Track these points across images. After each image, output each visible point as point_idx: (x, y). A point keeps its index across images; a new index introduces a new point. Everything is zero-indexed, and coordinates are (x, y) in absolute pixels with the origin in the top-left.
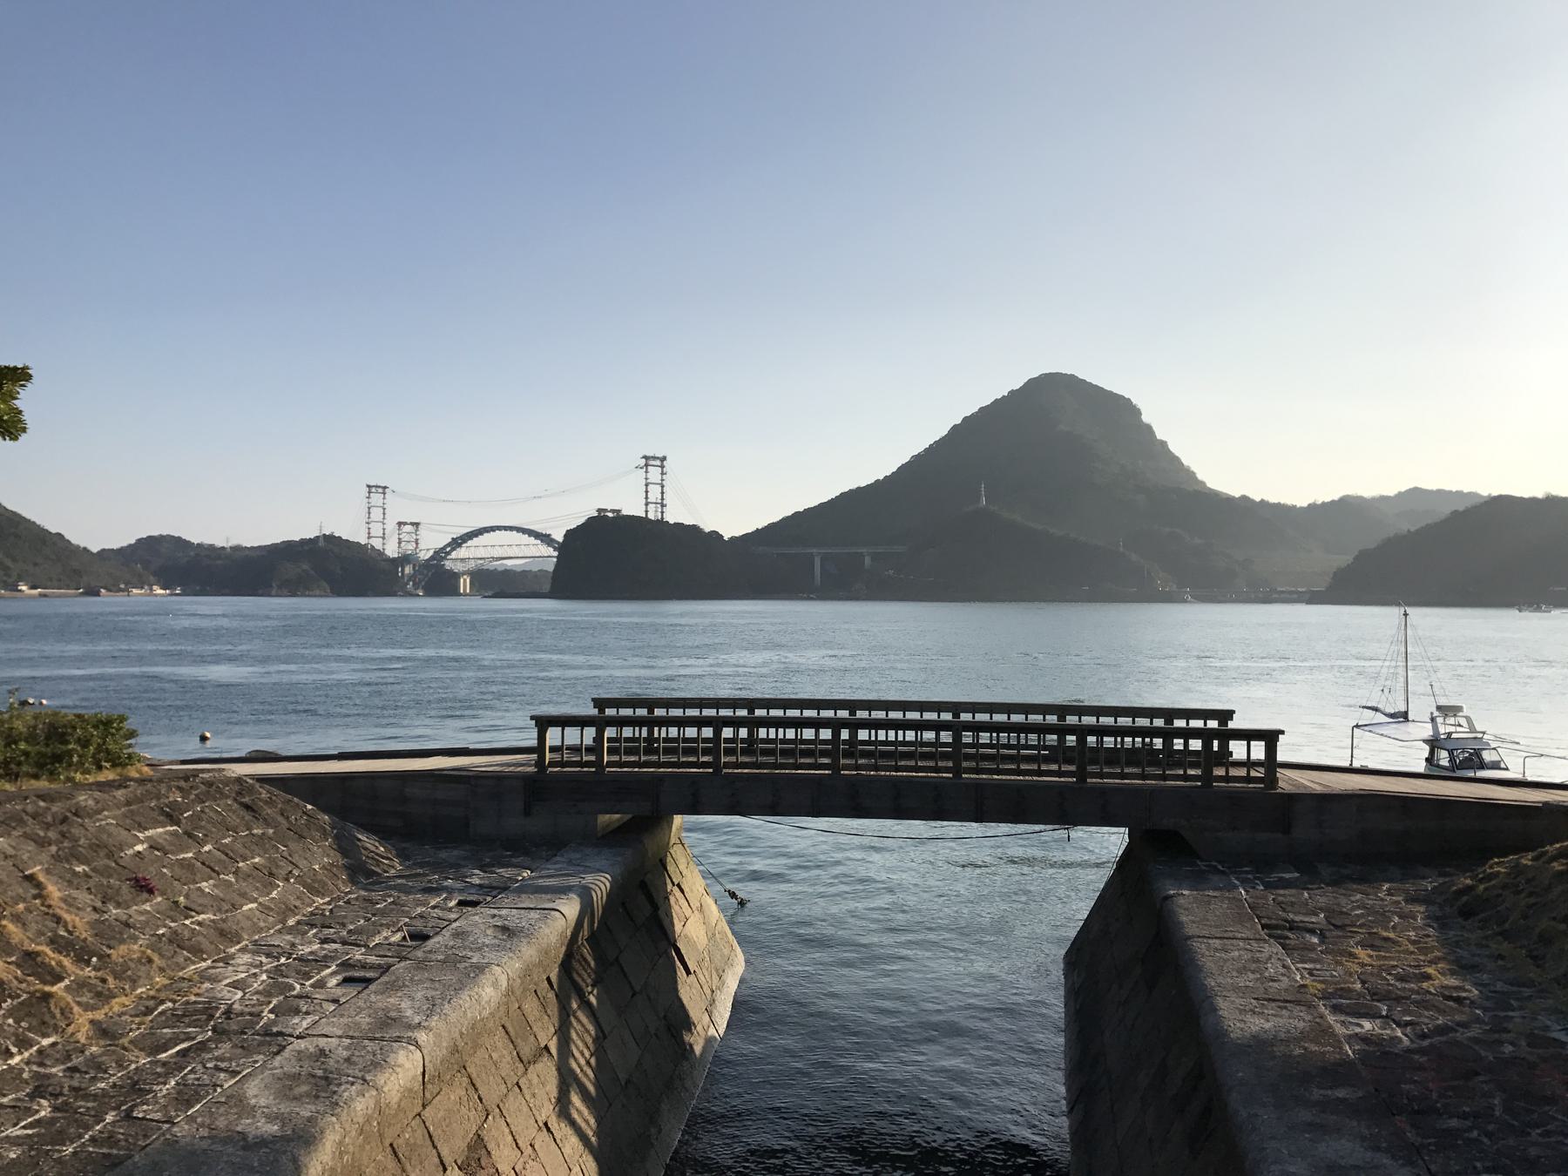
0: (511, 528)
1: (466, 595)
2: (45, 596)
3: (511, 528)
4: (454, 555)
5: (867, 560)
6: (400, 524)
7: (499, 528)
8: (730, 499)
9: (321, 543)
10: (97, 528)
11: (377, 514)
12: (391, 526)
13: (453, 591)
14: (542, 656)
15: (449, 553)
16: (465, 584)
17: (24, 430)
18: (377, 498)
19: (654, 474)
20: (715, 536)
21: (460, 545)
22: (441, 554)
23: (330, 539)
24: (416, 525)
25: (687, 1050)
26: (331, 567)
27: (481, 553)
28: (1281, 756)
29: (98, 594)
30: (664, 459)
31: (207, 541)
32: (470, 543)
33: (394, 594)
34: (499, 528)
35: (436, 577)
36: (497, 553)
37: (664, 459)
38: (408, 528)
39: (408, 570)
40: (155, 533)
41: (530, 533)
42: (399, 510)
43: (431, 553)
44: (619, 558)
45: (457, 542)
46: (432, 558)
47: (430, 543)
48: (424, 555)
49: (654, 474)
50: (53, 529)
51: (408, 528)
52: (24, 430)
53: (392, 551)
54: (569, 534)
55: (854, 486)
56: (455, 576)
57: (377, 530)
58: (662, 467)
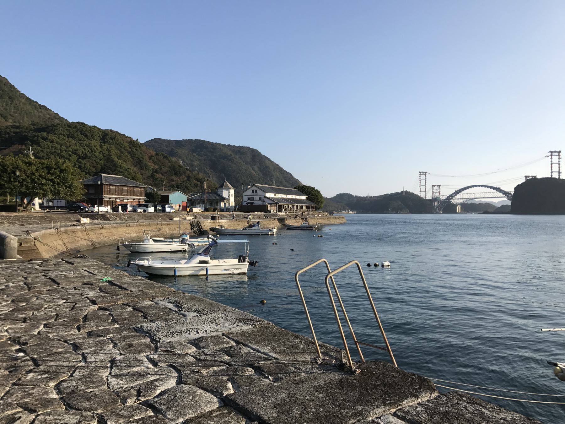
0: (482, 186)
1: (459, 213)
3: (482, 186)
4: (456, 197)
6: (433, 186)
7: (476, 186)
9: (404, 194)
11: (423, 183)
12: (429, 187)
13: (454, 212)
15: (454, 197)
16: (459, 208)
18: (423, 177)
19: (555, 159)
21: (458, 193)
22: (450, 197)
23: (406, 192)
24: (439, 186)
25: (369, 403)
27: (469, 196)
28: (209, 273)
30: (560, 152)
31: (359, 195)
32: (463, 192)
33: (433, 213)
34: (476, 186)
35: (447, 206)
36: (472, 196)
37: (560, 152)
38: (436, 187)
40: (342, 193)
41: (491, 187)
42: (431, 181)
45: (457, 192)
46: (447, 199)
47: (444, 194)
48: (443, 198)
49: (555, 159)
51: (436, 187)
53: (429, 196)
54: (518, 188)
56: (455, 206)
57: (423, 189)
58: (559, 155)
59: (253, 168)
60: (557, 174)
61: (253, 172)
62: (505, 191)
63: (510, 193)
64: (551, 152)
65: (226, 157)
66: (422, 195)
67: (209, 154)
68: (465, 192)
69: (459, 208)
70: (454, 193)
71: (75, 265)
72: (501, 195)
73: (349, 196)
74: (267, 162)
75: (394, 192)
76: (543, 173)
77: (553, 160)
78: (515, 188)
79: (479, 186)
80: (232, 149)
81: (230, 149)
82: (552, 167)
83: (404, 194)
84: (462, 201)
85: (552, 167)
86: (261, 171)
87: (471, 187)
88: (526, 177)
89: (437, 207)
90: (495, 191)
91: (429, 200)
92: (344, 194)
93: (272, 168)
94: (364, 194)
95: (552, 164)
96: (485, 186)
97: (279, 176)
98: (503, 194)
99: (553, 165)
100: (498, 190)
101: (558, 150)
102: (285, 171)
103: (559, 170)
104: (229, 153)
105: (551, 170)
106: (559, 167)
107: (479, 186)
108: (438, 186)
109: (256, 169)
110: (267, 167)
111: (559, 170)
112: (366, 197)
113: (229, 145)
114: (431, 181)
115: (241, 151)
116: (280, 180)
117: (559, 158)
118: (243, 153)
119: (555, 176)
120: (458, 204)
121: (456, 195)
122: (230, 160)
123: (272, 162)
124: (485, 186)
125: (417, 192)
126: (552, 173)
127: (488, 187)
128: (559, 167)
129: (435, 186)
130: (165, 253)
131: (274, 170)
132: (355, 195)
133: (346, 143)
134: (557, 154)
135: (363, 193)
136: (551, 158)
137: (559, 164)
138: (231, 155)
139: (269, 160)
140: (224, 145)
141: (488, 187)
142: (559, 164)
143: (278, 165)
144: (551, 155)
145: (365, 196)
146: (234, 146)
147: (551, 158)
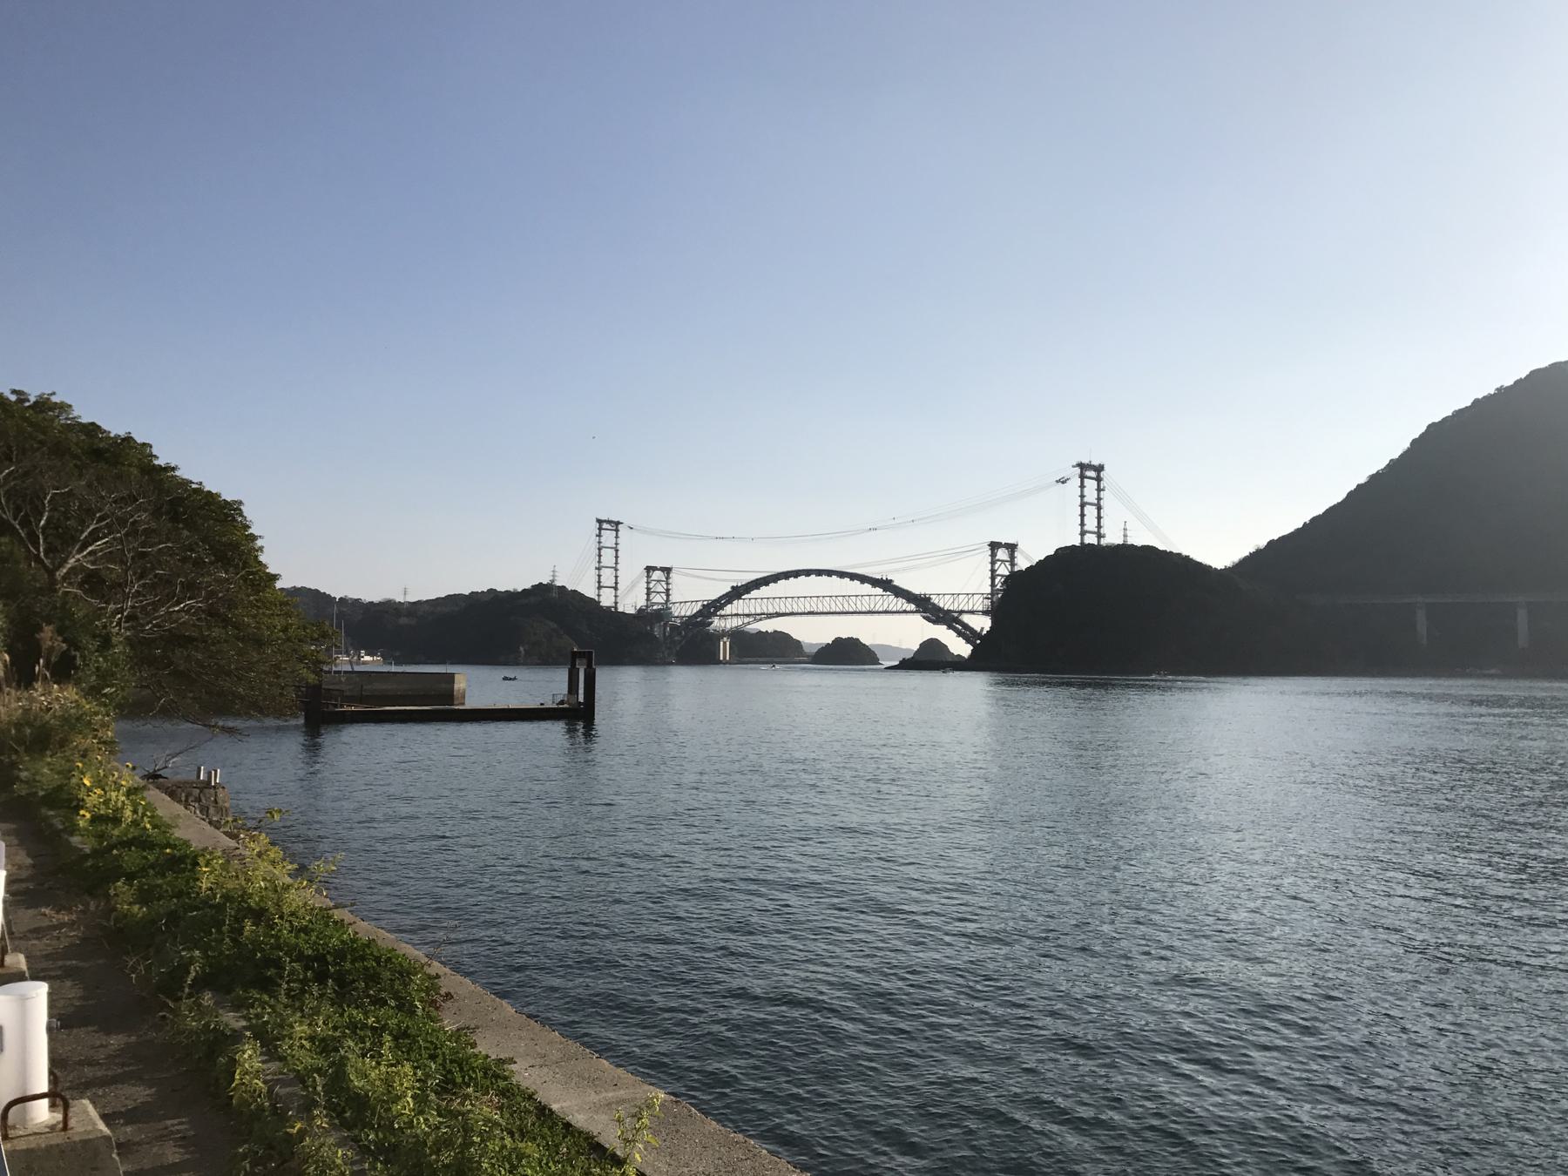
0: (829, 573)
1: (725, 663)
3: (829, 573)
4: (728, 609)
5: (1421, 618)
6: (649, 569)
7: (808, 573)
8: (1216, 514)
15: (722, 607)
18: (608, 537)
22: (713, 608)
24: (667, 571)
30: (1099, 469)
31: (353, 594)
32: (755, 593)
34: (808, 573)
37: (600, 521)
38: (657, 575)
41: (863, 579)
43: (698, 607)
44: (1089, 620)
45: (737, 593)
47: (687, 597)
49: (1091, 485)
53: (631, 601)
57: (607, 579)
58: (1099, 479)
64: (1082, 466)
66: (607, 600)
68: (764, 591)
70: (727, 595)
82: (1082, 515)
85: (1082, 515)
87: (786, 575)
90: (879, 591)
95: (1083, 505)
96: (842, 575)
98: (909, 601)
100: (886, 585)
101: (1095, 463)
103: (1099, 526)
105: (1082, 524)
106: (1099, 518)
107: (819, 573)
111: (1099, 526)
114: (636, 555)
117: (1099, 490)
119: (1091, 539)
121: (730, 602)
124: (842, 575)
125: (589, 591)
126: (1083, 533)
128: (1099, 518)
129: (654, 569)
130: (783, 610)
132: (337, 594)
134: (1092, 474)
135: (917, 592)
136: (1082, 486)
142: (1099, 508)
147: (1082, 486)
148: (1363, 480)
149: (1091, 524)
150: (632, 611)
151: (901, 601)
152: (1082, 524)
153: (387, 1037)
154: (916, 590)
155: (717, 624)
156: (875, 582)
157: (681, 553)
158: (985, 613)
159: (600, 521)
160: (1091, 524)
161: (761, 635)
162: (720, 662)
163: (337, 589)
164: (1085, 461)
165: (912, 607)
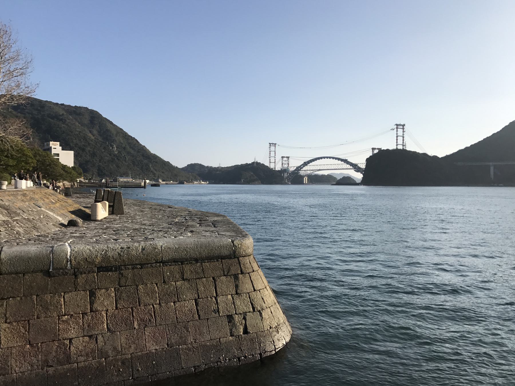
0: (330, 158)
1: (306, 184)
2: (167, 184)
3: (330, 158)
4: (304, 168)
5: (492, 169)
6: (282, 157)
7: (324, 158)
8: (439, 141)
9: (255, 165)
10: (179, 161)
11: (272, 154)
12: (278, 158)
14: (51, 213)
15: (302, 168)
16: (306, 180)
17: (63, 150)
18: (273, 148)
19: (400, 131)
20: (435, 157)
21: (306, 165)
22: (299, 168)
23: (258, 164)
24: (288, 157)
26: (254, 174)
29: (183, 183)
30: (404, 125)
31: (210, 165)
32: (311, 164)
34: (324, 158)
35: (295, 178)
37: (270, 144)
38: (285, 159)
39: (286, 175)
40: (193, 163)
41: (339, 159)
42: (281, 152)
43: (295, 168)
45: (306, 164)
46: (295, 170)
47: (293, 165)
48: (292, 169)
49: (400, 131)
50: (166, 160)
52: (63, 150)
55: (485, 137)
56: (302, 177)
57: (272, 160)
58: (403, 129)
59: (90, 132)
60: (402, 146)
61: (90, 135)
62: (351, 163)
63: (187, 182)
64: (397, 125)
65: (57, 117)
66: (272, 166)
67: (35, 112)
68: (313, 163)
69: (306, 180)
70: (303, 165)
71: (42, 209)
72: (348, 166)
73: (201, 166)
74: (108, 125)
75: (244, 163)
76: (389, 144)
77: (398, 132)
78: (367, 160)
79: (327, 158)
80: (66, 108)
81: (64, 109)
82: (397, 140)
83: (255, 165)
84: (309, 172)
85: (397, 140)
86: (100, 135)
88: (373, 149)
89: (286, 178)
90: (343, 163)
91: (279, 171)
92: (195, 164)
93: (114, 132)
94: (215, 165)
95: (397, 137)
96: (333, 158)
97: (122, 141)
99: (398, 138)
100: (346, 161)
101: (402, 124)
102: (130, 136)
104: (61, 112)
105: (397, 142)
106: (403, 140)
107: (327, 158)
108: (287, 157)
109: (95, 132)
110: (108, 130)
111: (403, 143)
112: (218, 168)
113: (62, 105)
114: (281, 152)
115: (77, 112)
116: (124, 146)
117: (403, 132)
118: (80, 114)
119: (400, 147)
120: (305, 176)
121: (304, 166)
122: (61, 120)
123: (115, 125)
125: (267, 164)
126: (397, 145)
127: (336, 159)
128: (403, 140)
129: (284, 157)
131: (116, 135)
132: (206, 165)
133: (185, 129)
134: (401, 127)
136: (397, 131)
137: (403, 137)
138: (63, 114)
139: (111, 123)
140: (57, 104)
141: (336, 159)
142: (403, 137)
143: (121, 129)
144: (397, 128)
145: (216, 167)
146: (69, 106)
147: (397, 131)
148: (507, 124)
149: (400, 141)
150: (280, 169)
151: (348, 165)
152: (397, 142)
153: (30, 154)
154: (354, 162)
155: (302, 173)
156: (342, 160)
157: (291, 151)
158: (27, 187)
159: (270, 144)
160: (400, 141)
161: (323, 176)
162: (304, 184)
163: (206, 164)
164: (398, 123)
165: (351, 167)
